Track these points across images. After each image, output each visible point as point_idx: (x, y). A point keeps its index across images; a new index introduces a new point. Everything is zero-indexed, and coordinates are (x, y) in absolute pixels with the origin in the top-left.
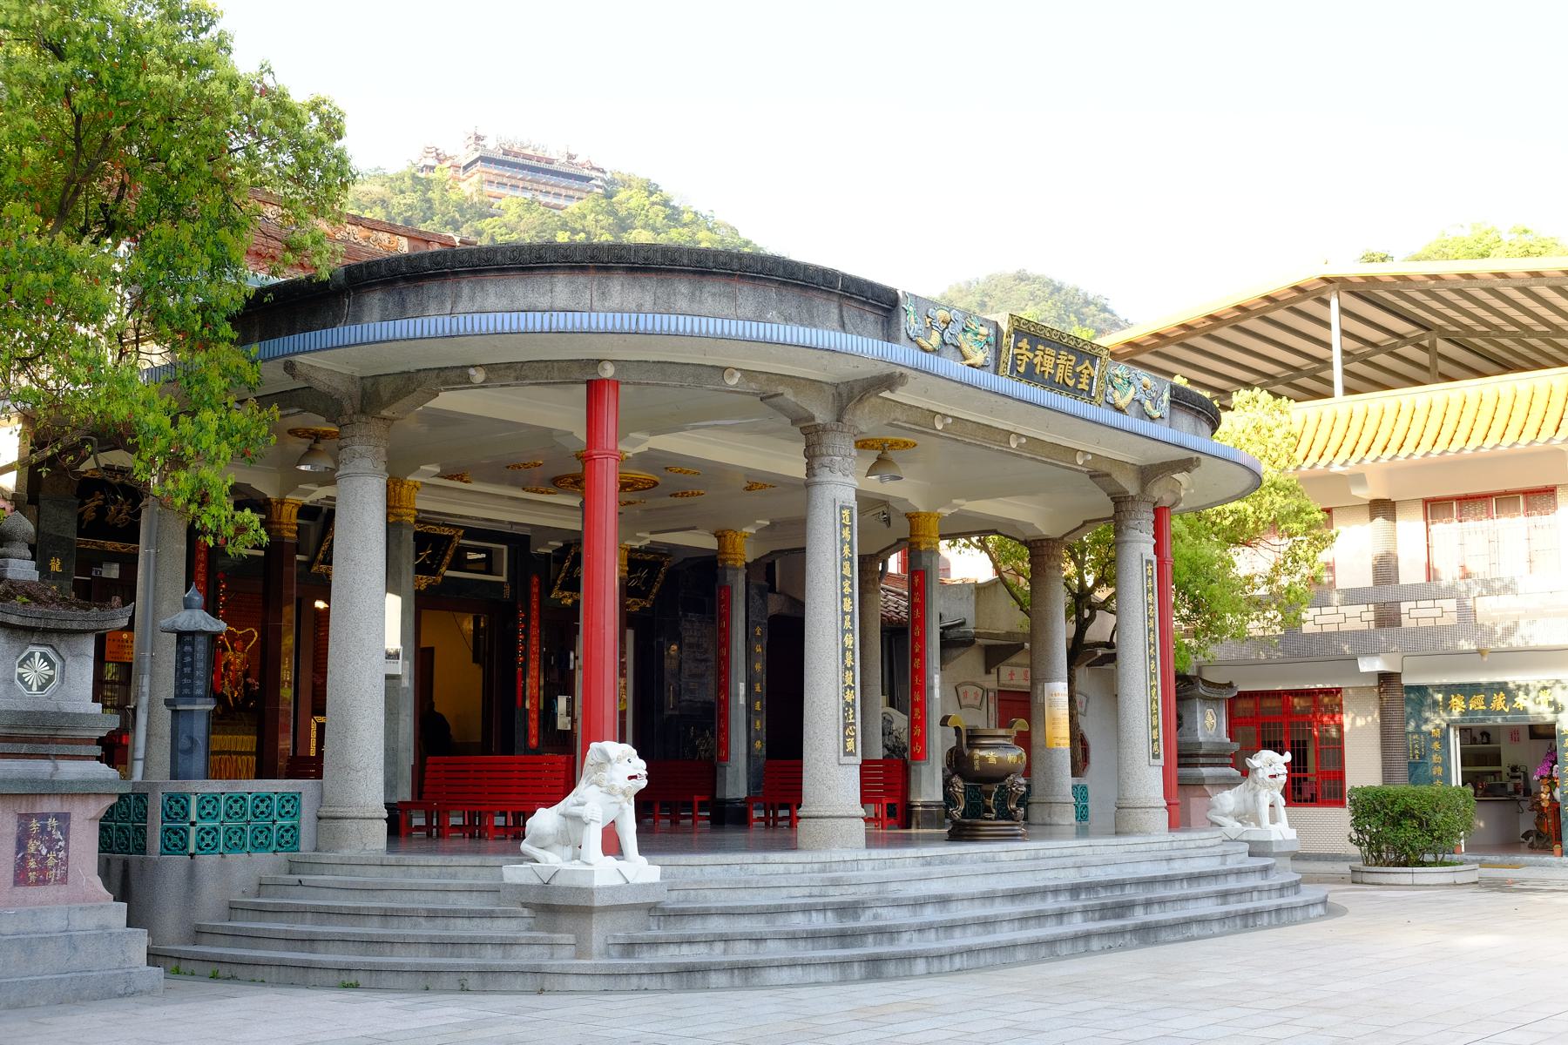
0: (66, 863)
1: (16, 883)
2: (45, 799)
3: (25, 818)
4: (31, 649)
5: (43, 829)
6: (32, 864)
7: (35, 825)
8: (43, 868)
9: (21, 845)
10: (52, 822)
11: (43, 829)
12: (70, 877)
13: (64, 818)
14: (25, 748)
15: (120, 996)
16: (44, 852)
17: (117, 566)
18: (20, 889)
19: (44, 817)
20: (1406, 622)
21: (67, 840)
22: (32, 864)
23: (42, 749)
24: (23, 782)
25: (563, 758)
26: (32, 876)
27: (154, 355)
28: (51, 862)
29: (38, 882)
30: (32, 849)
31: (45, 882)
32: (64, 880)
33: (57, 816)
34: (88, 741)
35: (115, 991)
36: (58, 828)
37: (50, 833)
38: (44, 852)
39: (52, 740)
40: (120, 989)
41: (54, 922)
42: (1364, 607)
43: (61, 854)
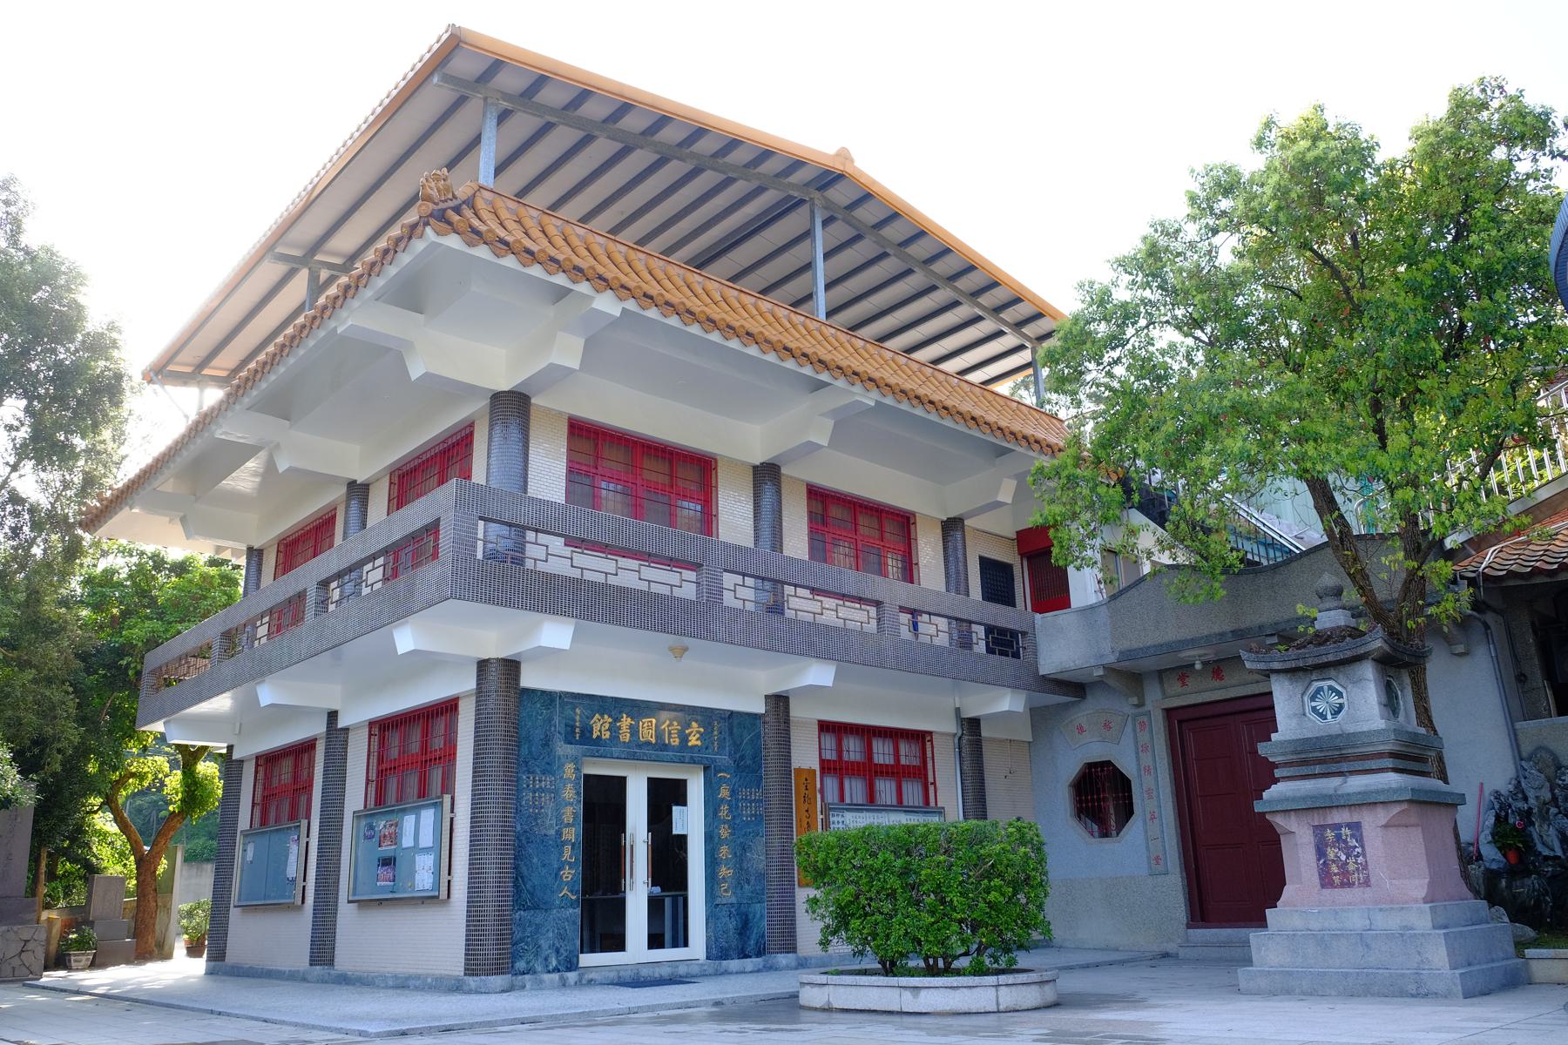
0: (1365, 867)
1: (1323, 886)
2: (1335, 811)
3: (1319, 830)
4: (1317, 684)
5: (1338, 837)
6: (1334, 869)
7: (1330, 834)
8: (1344, 872)
9: (1321, 852)
10: (1345, 831)
11: (1338, 837)
12: (1373, 880)
13: (1356, 827)
14: (1318, 769)
15: (1413, 996)
16: (1343, 858)
17: (401, 651)
18: (1327, 892)
19: (1337, 827)
20: (789, 614)
21: (1363, 847)
22: (1334, 869)
23: (1334, 768)
24: (1304, 798)
25: (452, 960)
26: (1336, 879)
27: (33, 367)
28: (1351, 867)
29: (1343, 885)
30: (1331, 856)
31: (1350, 885)
32: (1367, 883)
33: (1349, 826)
34: (1380, 755)
35: (1409, 989)
36: (1352, 836)
37: (1345, 842)
38: (1343, 858)
39: (1344, 758)
40: (1412, 988)
41: (1356, 921)
42: (541, 567)
43: (1360, 859)
